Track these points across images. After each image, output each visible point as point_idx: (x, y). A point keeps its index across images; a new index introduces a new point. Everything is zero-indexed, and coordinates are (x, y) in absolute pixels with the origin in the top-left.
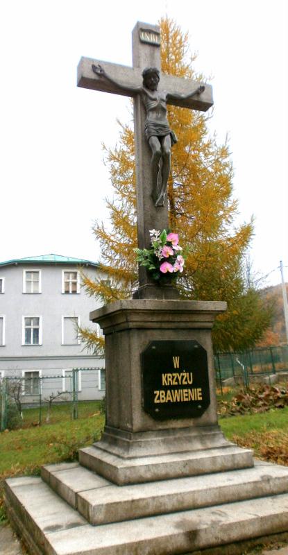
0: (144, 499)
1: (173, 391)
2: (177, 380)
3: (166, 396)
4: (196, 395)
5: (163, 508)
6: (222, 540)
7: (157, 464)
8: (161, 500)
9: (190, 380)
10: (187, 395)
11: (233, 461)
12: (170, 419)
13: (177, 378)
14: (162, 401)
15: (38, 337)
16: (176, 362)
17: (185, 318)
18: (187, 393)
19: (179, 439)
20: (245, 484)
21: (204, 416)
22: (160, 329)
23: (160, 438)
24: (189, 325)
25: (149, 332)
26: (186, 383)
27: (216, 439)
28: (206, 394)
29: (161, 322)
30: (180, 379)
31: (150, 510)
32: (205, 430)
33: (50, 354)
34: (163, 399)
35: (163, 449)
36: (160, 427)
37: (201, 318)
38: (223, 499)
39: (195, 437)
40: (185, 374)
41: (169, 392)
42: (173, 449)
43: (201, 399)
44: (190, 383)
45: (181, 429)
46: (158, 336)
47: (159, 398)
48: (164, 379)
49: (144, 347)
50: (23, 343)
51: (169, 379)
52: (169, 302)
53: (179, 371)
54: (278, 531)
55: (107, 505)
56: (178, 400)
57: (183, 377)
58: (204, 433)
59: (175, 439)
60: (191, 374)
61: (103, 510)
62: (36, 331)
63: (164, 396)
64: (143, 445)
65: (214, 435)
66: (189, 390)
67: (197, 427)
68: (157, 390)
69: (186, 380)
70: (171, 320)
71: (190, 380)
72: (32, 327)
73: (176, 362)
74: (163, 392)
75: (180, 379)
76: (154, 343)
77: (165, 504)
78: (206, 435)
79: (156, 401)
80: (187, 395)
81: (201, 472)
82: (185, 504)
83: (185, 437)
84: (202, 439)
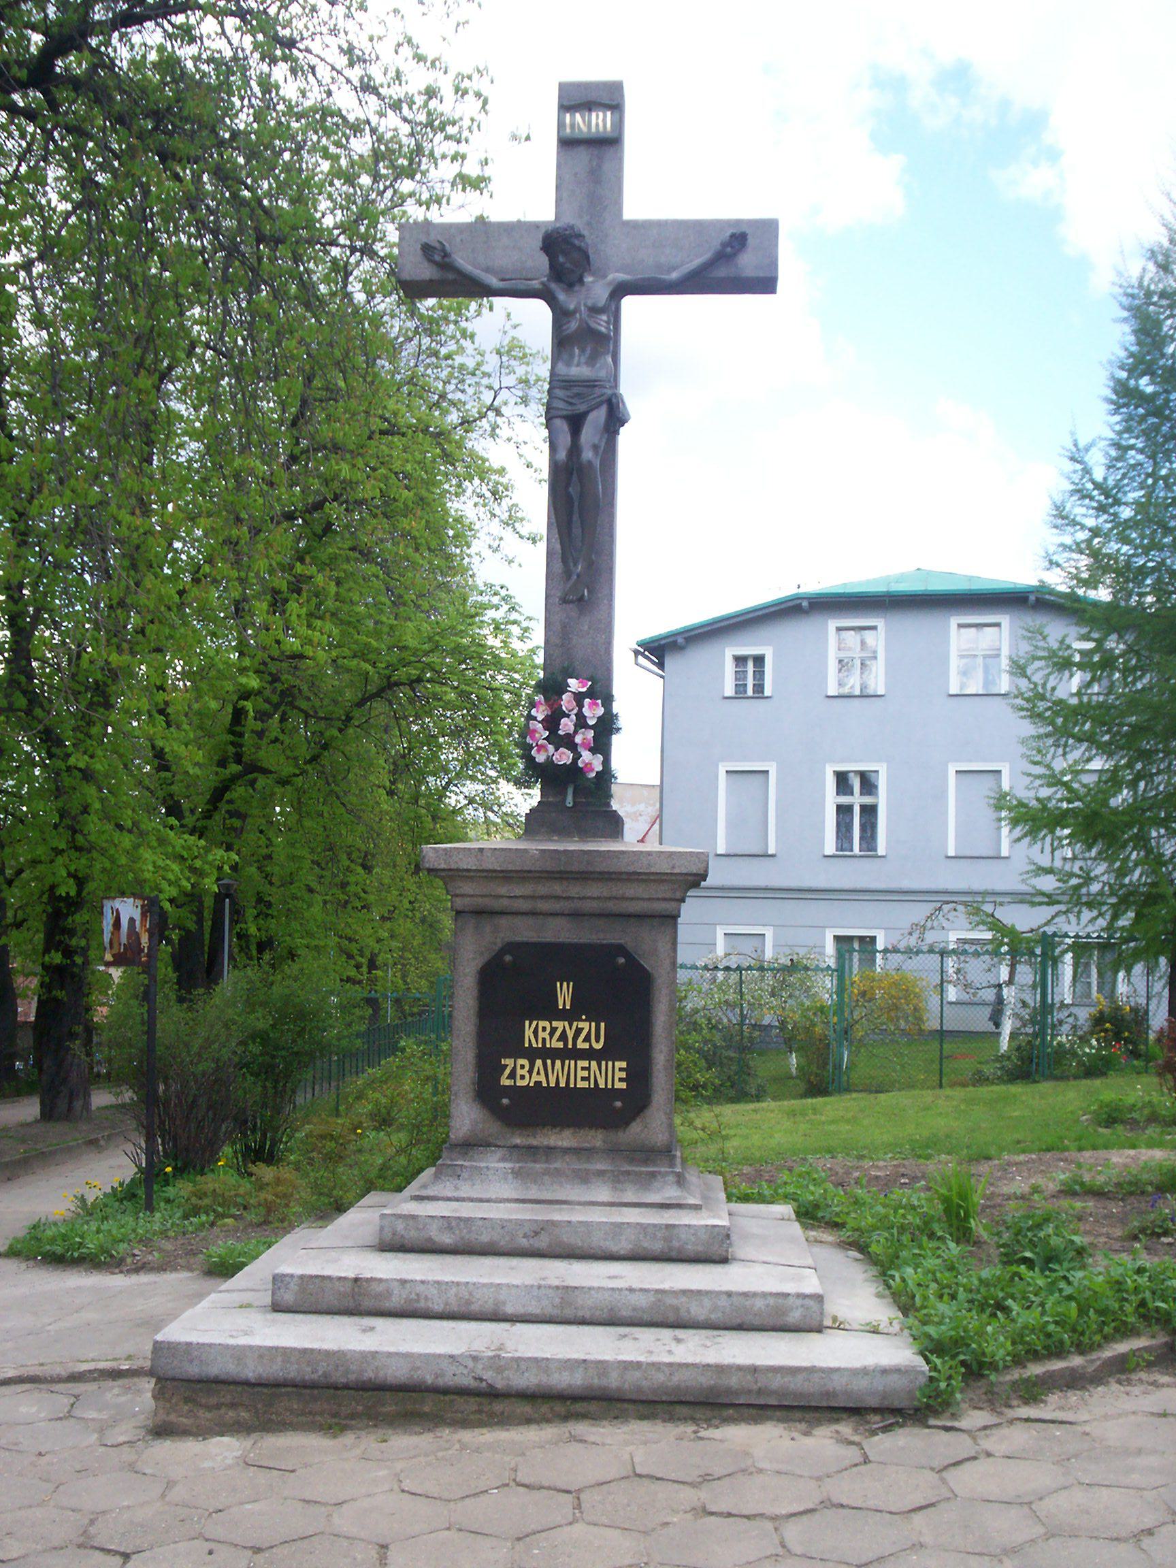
0: (380, 1280)
1: (549, 1062)
2: (563, 1037)
3: (530, 1072)
4: (614, 1075)
5: (422, 1304)
6: (490, 1386)
7: (468, 1219)
8: (421, 1288)
9: (597, 1040)
10: (585, 1074)
11: (667, 1239)
12: (544, 1126)
13: (564, 1031)
14: (520, 1083)
15: (874, 826)
16: (564, 995)
17: (594, 890)
18: (588, 1069)
19: (558, 1173)
20: (631, 1290)
21: (635, 1127)
22: (533, 913)
23: (508, 1165)
24: (612, 906)
25: (503, 921)
26: (586, 1046)
27: (656, 1184)
28: (639, 1076)
29: (532, 897)
30: (570, 1034)
31: (395, 1302)
32: (632, 1161)
33: (906, 884)
34: (522, 1077)
35: (508, 1189)
36: (518, 1141)
37: (631, 890)
38: (658, 1318)
39: (601, 1173)
40: (585, 1025)
41: (539, 1063)
42: (533, 1193)
43: (623, 1085)
44: (598, 1046)
45: (566, 1151)
46: (525, 932)
47: (512, 1075)
48: (529, 1033)
49: (487, 956)
50: (830, 847)
51: (541, 1035)
52: (543, 851)
53: (569, 1016)
54: (651, 1397)
55: (302, 1277)
56: (562, 1084)
57: (579, 1031)
58: (628, 1168)
59: (547, 1172)
60: (603, 1025)
61: (293, 1286)
62: (869, 812)
63: (525, 1072)
64: (465, 1175)
65: (653, 1175)
66: (594, 1063)
67: (614, 1151)
68: (510, 1057)
69: (587, 1039)
70: (605, 894)
71: (597, 1040)
72: (857, 800)
73: (564, 995)
74: (525, 1062)
75: (570, 1034)
76: (510, 947)
77: (426, 1298)
78: (628, 1173)
79: (505, 1081)
80: (585, 1074)
81: (577, 1251)
82: (475, 1308)
83: (574, 1171)
84: (617, 1179)
